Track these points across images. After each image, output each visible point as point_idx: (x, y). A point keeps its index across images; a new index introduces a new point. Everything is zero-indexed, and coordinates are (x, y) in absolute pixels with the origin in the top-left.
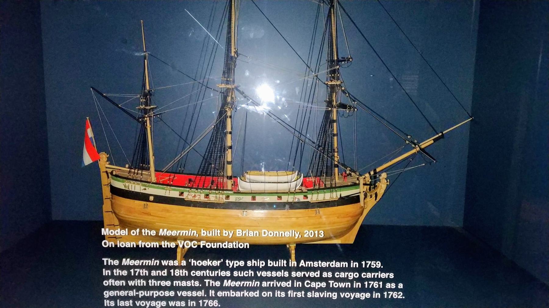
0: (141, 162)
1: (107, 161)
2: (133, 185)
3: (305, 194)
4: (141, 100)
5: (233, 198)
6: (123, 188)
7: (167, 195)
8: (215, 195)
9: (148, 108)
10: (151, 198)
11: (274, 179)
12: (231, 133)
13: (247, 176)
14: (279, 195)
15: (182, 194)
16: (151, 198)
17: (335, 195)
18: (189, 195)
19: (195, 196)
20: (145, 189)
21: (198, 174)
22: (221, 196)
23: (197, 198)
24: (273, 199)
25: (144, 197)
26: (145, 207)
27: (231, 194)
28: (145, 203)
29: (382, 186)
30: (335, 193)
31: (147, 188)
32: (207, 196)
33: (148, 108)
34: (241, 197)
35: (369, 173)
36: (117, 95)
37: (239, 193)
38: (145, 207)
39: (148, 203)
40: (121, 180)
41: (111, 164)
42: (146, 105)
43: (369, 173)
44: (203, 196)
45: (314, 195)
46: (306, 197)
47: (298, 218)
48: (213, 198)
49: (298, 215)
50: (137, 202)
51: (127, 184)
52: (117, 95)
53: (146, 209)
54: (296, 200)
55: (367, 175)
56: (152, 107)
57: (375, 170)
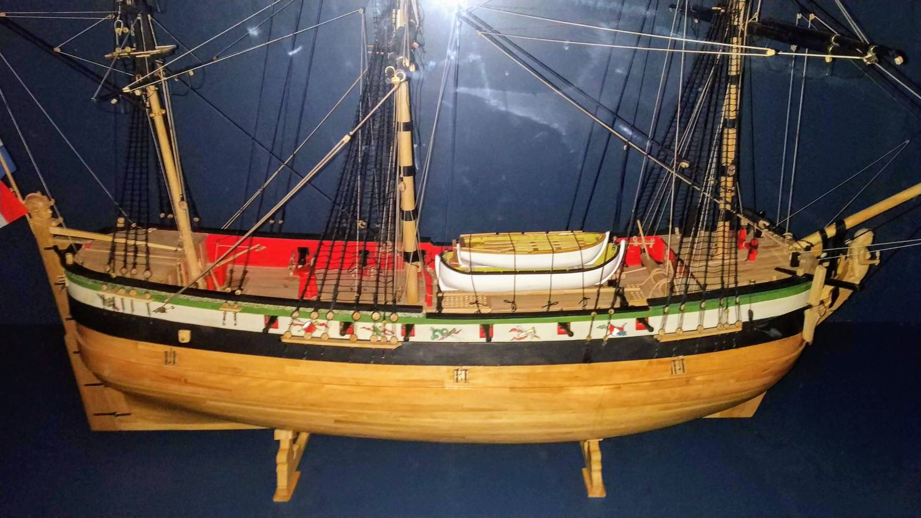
0: (153, 214)
1: (54, 216)
2: (127, 300)
3: (641, 314)
4: (118, 31)
5: (424, 333)
6: (98, 304)
7: (230, 325)
8: (370, 325)
9: (145, 54)
10: (185, 336)
11: (543, 261)
12: (411, 171)
13: (463, 255)
14: (564, 319)
15: (272, 321)
16: (185, 336)
17: (735, 315)
18: (290, 327)
19: (311, 329)
20: (163, 310)
21: (326, 236)
22: (389, 326)
23: (317, 333)
24: (546, 332)
25: (162, 332)
26: (168, 359)
27: (420, 322)
28: (168, 348)
29: (856, 265)
30: (732, 309)
31: (168, 306)
32: (347, 327)
33: (145, 54)
34: (449, 326)
35: (823, 233)
36: (42, 15)
37: (438, 316)
38: (168, 359)
39: (175, 349)
40: (90, 282)
41: (70, 223)
42: (139, 48)
43: (823, 233)
44: (334, 329)
45: (670, 317)
46: (643, 323)
47: (618, 387)
48: (365, 331)
49: (619, 379)
50: (144, 346)
51: (108, 296)
52: (42, 15)
53: (170, 367)
54: (615, 334)
55: (816, 238)
56: (158, 49)
57: (840, 223)
